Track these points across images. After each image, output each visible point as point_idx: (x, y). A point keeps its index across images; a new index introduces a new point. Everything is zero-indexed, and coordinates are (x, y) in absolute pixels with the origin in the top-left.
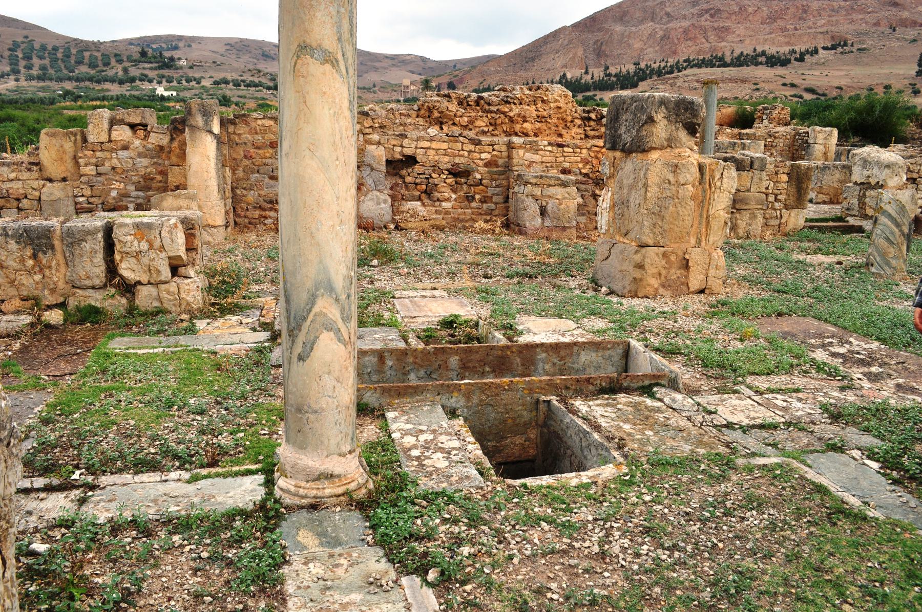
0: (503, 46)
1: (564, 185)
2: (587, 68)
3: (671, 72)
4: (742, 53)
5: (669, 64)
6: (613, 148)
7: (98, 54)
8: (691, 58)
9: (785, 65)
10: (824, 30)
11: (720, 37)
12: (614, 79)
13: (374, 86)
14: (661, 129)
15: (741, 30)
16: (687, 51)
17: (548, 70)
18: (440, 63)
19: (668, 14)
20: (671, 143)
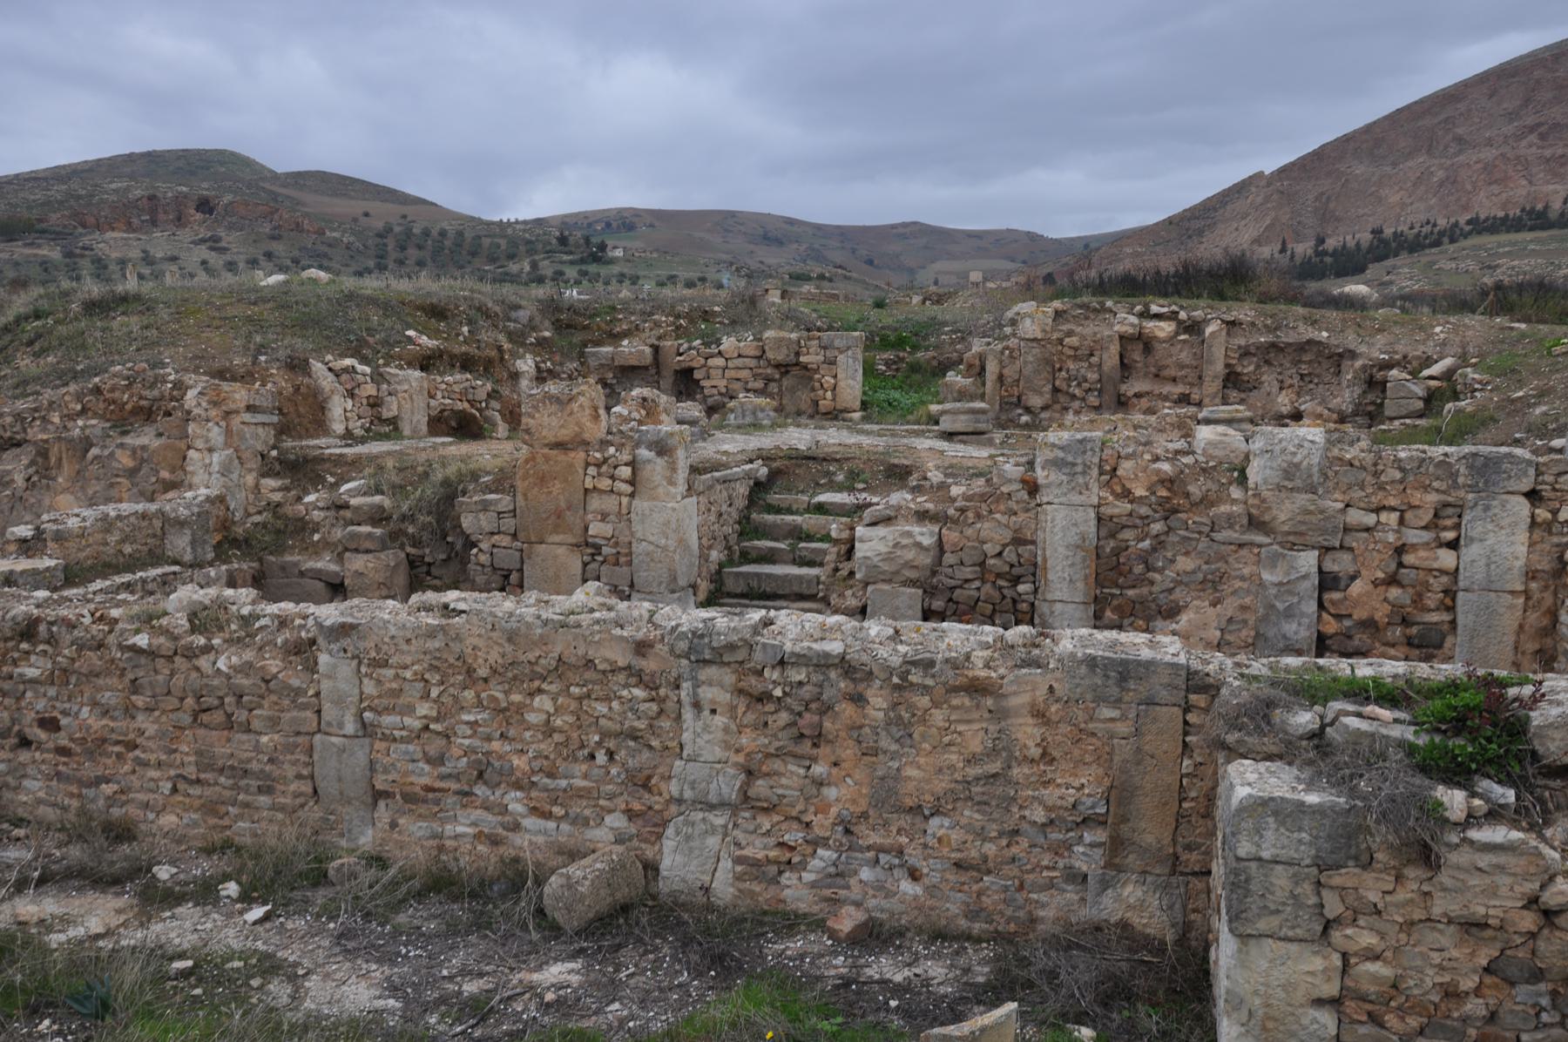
0: (282, 163)
2: (1284, 243)
3: (1437, 243)
5: (1436, 230)
7: (503, 243)
16: (1487, 205)
18: (1058, 242)
19: (1459, 140)
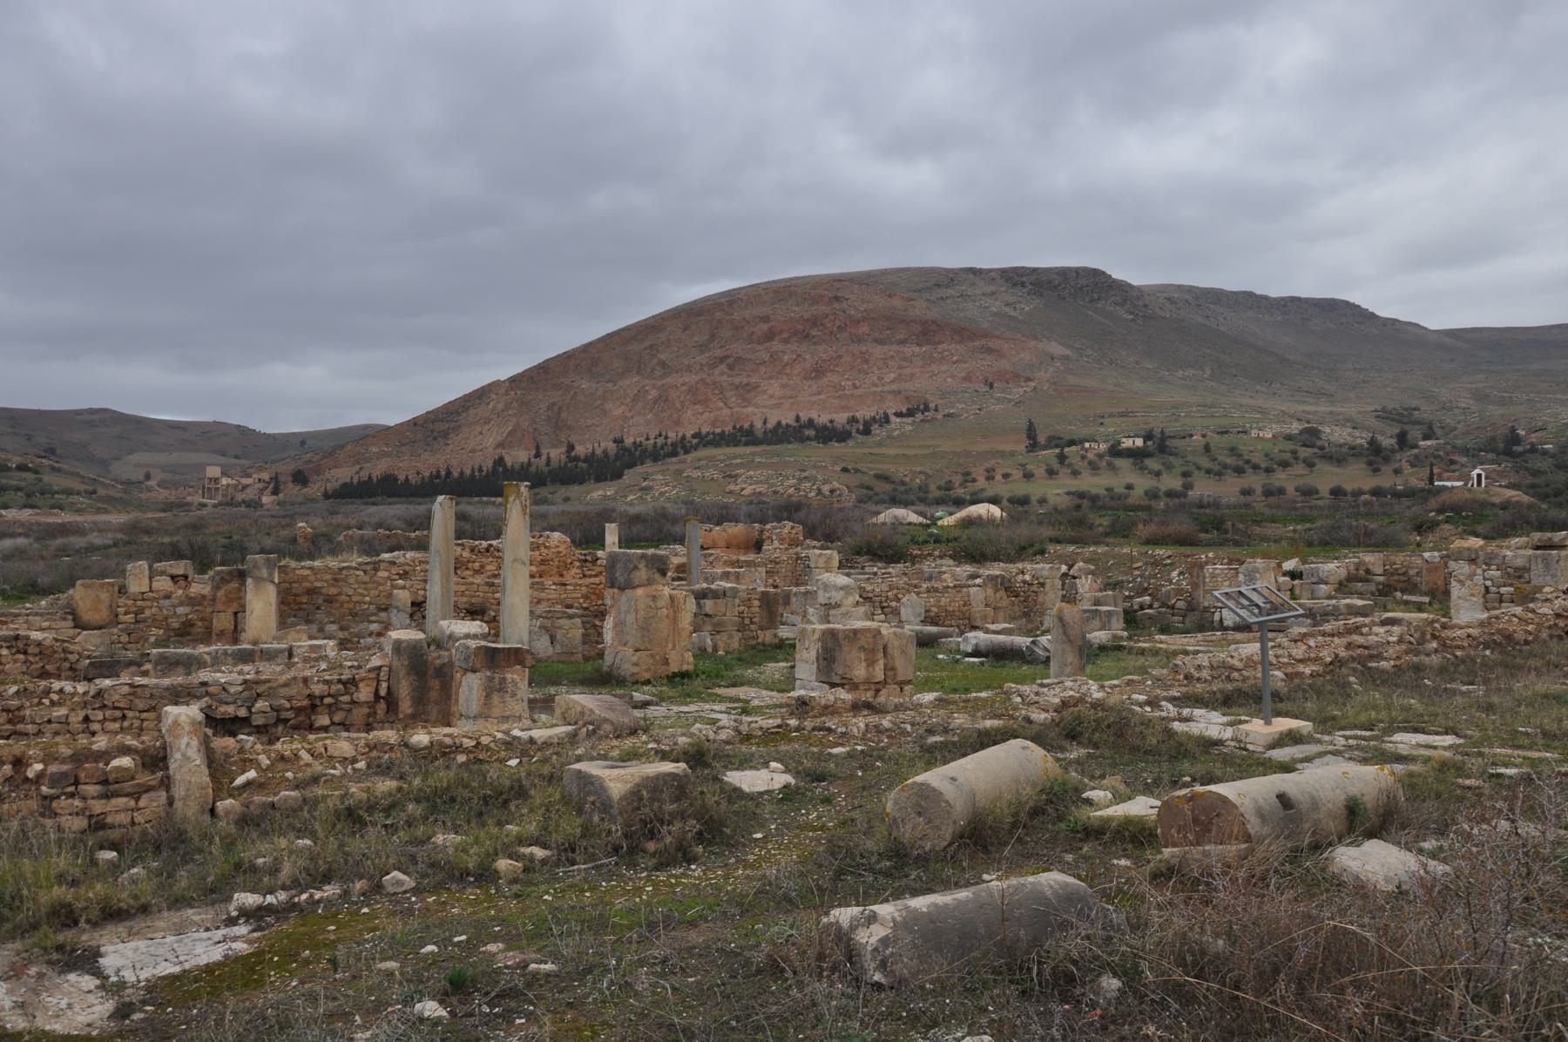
1: (571, 617)
2: (538, 448)
3: (674, 454)
4: (779, 423)
6: (612, 587)
8: (704, 431)
9: (843, 440)
10: (895, 387)
11: (744, 400)
12: (585, 465)
13: (148, 477)
14: (642, 573)
15: (774, 388)
16: (695, 421)
17: (473, 451)
19: (663, 364)
20: (650, 582)
